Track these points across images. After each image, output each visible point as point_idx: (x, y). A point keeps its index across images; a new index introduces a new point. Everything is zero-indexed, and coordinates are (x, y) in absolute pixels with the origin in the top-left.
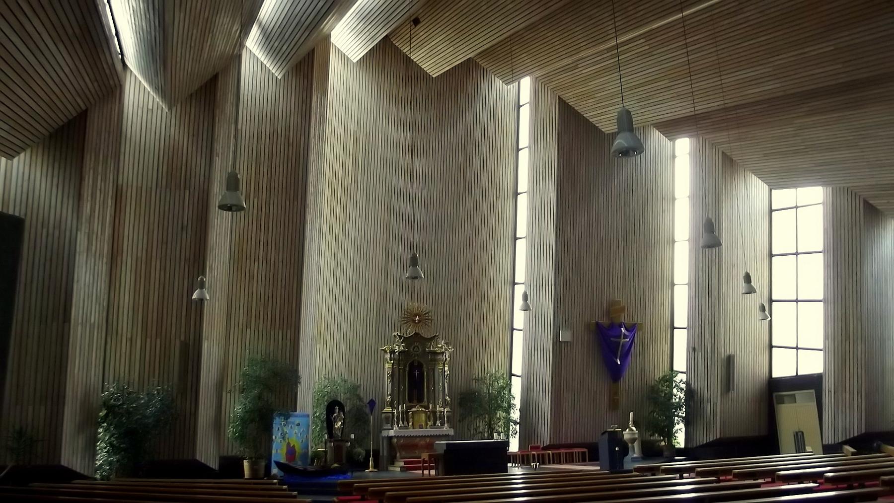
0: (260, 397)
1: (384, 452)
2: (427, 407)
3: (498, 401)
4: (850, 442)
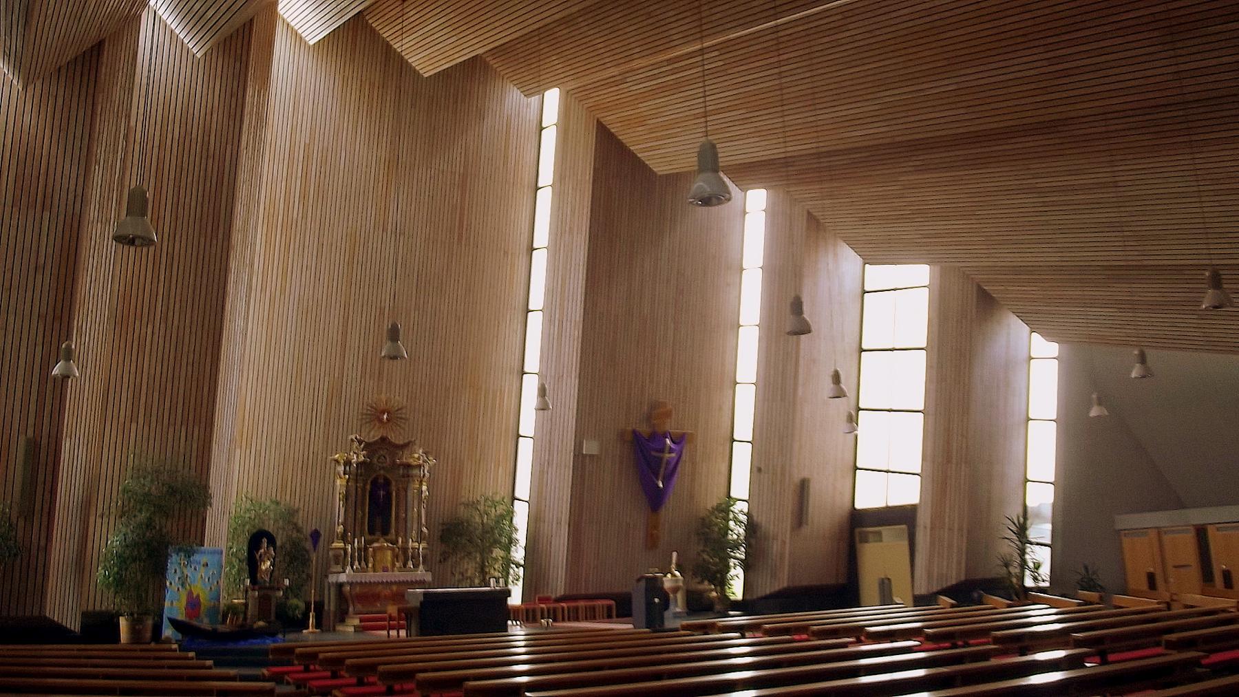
0: (149, 525)
1: (331, 606)
2: (395, 542)
3: (495, 534)
4: (946, 592)
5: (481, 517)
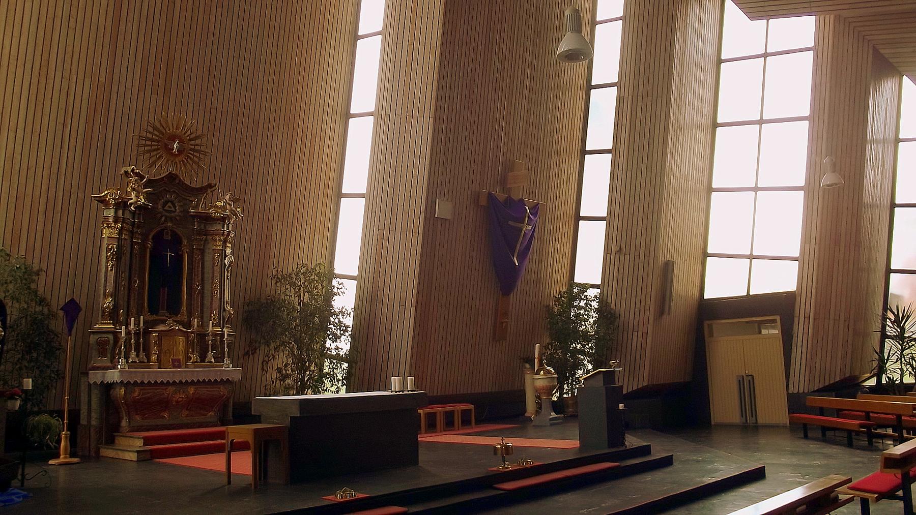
1: (91, 416)
2: (188, 325)
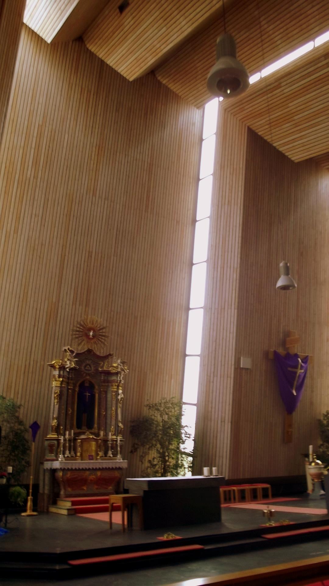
1: (45, 489)
2: (98, 435)
5: (161, 416)
